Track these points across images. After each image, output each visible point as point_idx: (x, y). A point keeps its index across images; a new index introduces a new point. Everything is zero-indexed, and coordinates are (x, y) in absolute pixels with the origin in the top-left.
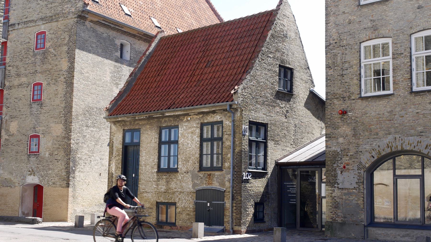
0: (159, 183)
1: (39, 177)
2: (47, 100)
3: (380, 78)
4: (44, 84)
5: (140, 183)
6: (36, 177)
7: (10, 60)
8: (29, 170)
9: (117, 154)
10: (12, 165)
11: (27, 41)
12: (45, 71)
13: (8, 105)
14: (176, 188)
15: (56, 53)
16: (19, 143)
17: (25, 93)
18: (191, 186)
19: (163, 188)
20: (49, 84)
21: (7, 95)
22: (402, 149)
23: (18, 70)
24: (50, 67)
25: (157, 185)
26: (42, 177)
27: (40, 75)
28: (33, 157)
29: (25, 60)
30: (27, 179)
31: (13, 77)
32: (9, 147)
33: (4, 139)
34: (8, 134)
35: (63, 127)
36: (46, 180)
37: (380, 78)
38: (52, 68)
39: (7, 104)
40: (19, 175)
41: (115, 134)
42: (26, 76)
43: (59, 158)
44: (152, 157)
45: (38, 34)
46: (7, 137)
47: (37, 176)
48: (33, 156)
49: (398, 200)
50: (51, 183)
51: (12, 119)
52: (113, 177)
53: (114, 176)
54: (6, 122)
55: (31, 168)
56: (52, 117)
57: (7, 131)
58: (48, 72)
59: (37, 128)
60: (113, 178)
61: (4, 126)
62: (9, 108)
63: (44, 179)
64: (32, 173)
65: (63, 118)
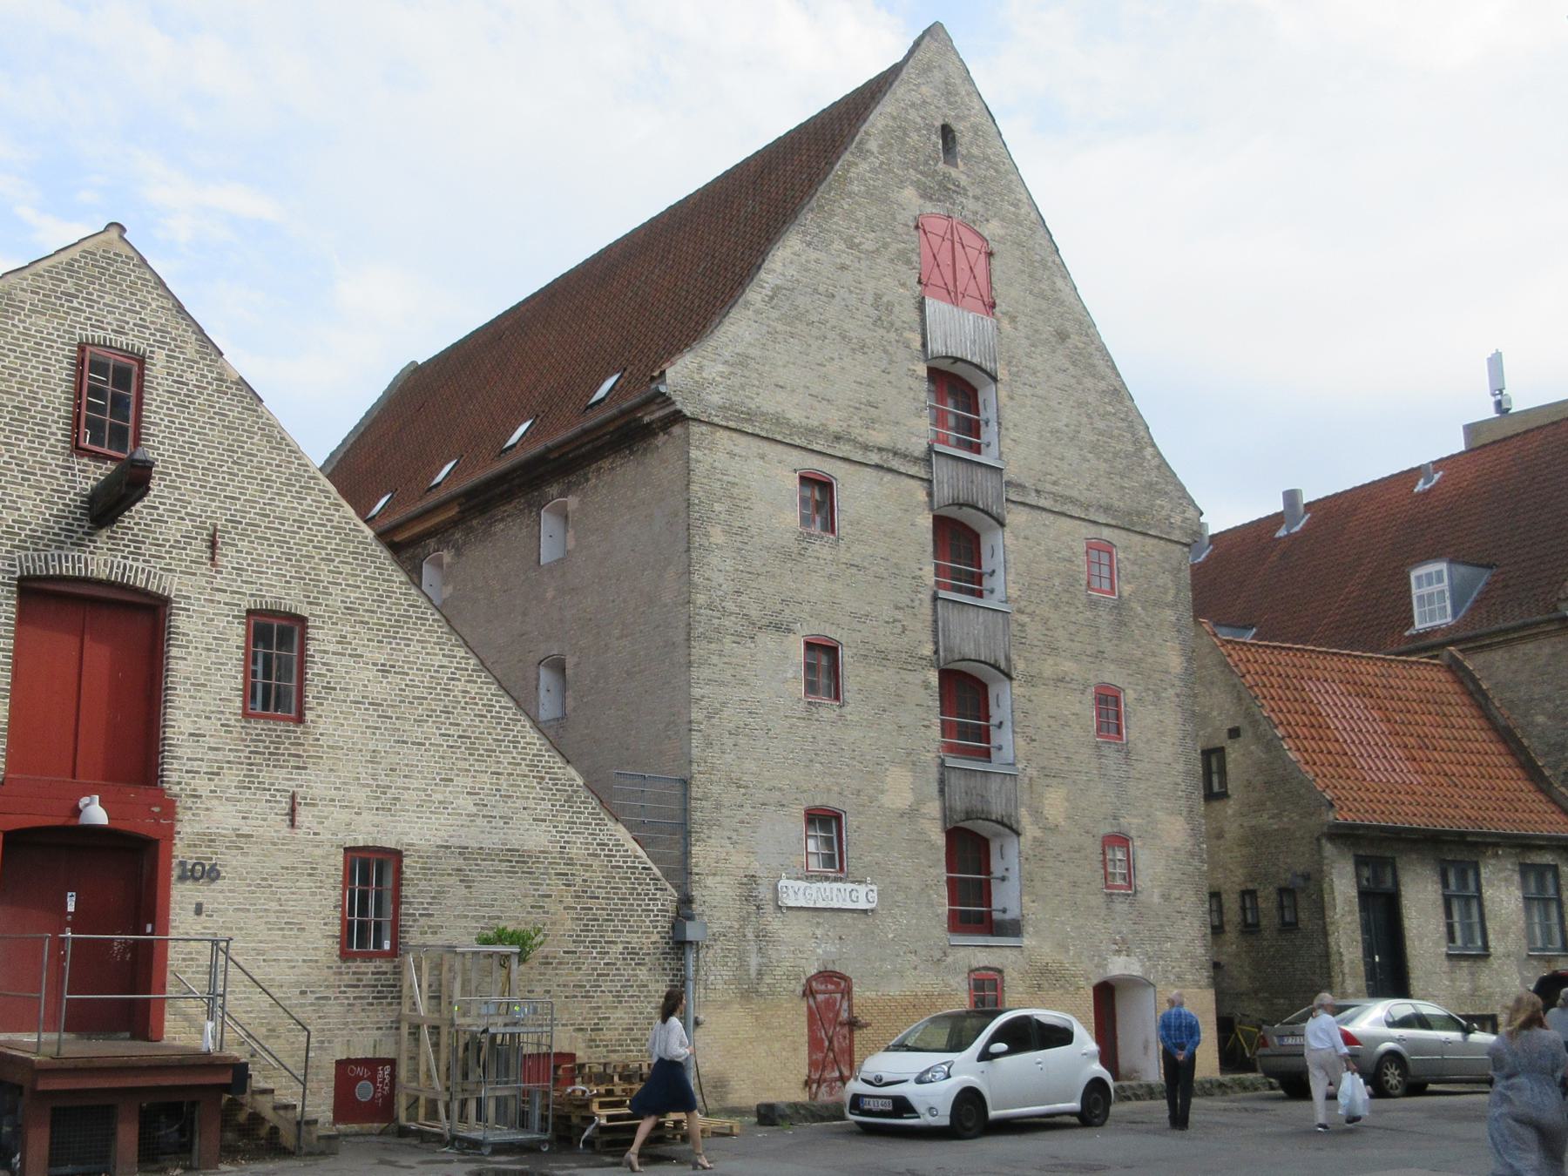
0: (1453, 975)
1: (1140, 961)
2: (1141, 745)
3: (111, 424)
4: (1128, 697)
5: (1412, 975)
6: (1133, 959)
7: (1019, 593)
8: (1115, 940)
9: (1346, 909)
10: (1062, 923)
11: (1066, 553)
12: (1127, 662)
13: (1030, 731)
14: (1489, 987)
15: (1149, 620)
16: (1077, 855)
17: (1077, 708)
18: (1518, 982)
19: (1466, 987)
20: (1139, 700)
21: (1022, 699)
22: (308, 639)
23: (1050, 633)
24: (1138, 653)
25: (1452, 980)
26: (1149, 959)
27: (1112, 667)
28: (1121, 903)
29: (1066, 609)
30: (1110, 966)
31: (1036, 650)
32: (1050, 865)
33: (1030, 838)
34: (1041, 825)
35: (1187, 826)
36: (1160, 967)
37: (111, 424)
38: (1142, 656)
39: (1026, 730)
40: (1086, 953)
41: (1334, 862)
42: (1075, 657)
43: (1186, 909)
44: (1433, 921)
45: (112, 224)
46: (1038, 833)
47: (1138, 957)
48: (1120, 899)
49: (81, 707)
50: (1172, 977)
51: (1049, 781)
52: (1343, 962)
53: (1344, 959)
54: (1031, 785)
55: (1119, 933)
56: (1158, 795)
57: (1037, 813)
58: (1134, 667)
59: (1122, 819)
60: (1345, 965)
61: (1026, 797)
62: (1035, 744)
63: (1155, 966)
64: (1123, 947)
65: (1182, 802)
